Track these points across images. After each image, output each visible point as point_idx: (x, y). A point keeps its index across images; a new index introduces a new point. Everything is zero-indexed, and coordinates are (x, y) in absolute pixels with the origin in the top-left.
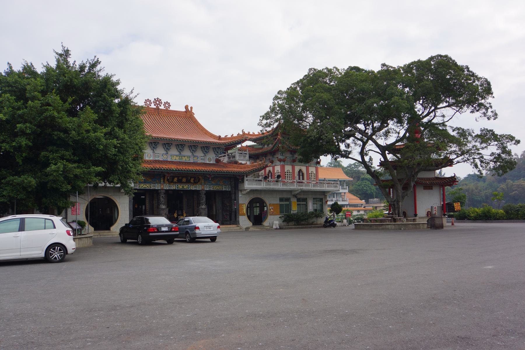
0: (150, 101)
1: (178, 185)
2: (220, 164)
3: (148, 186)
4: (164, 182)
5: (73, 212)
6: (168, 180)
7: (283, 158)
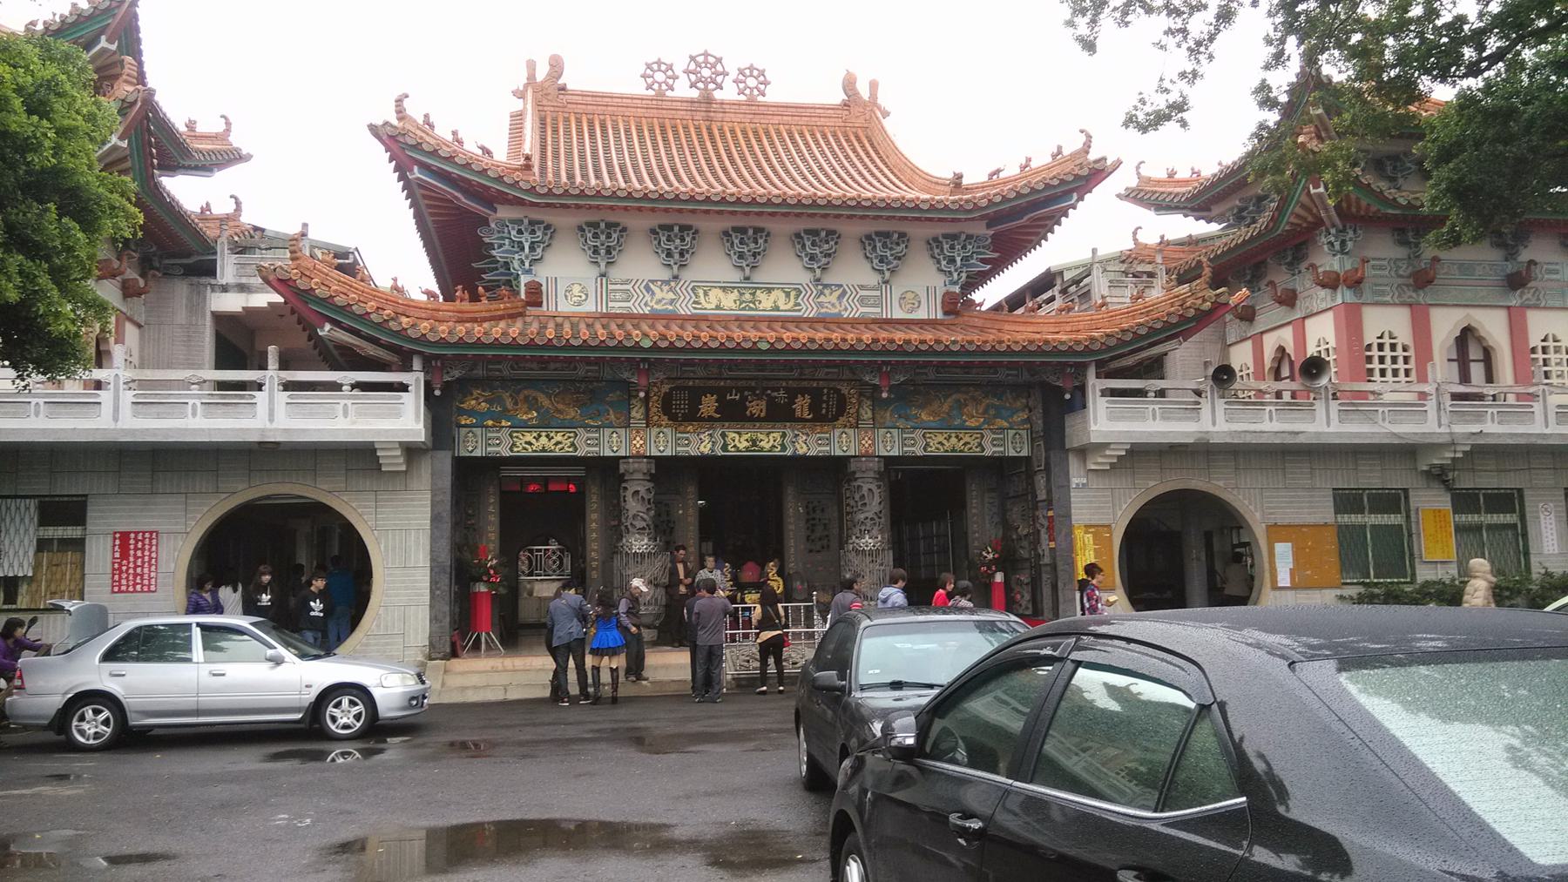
1: (724, 435)
2: (966, 319)
3: (557, 443)
4: (647, 418)
5: (120, 578)
6: (667, 409)
7: (1348, 267)
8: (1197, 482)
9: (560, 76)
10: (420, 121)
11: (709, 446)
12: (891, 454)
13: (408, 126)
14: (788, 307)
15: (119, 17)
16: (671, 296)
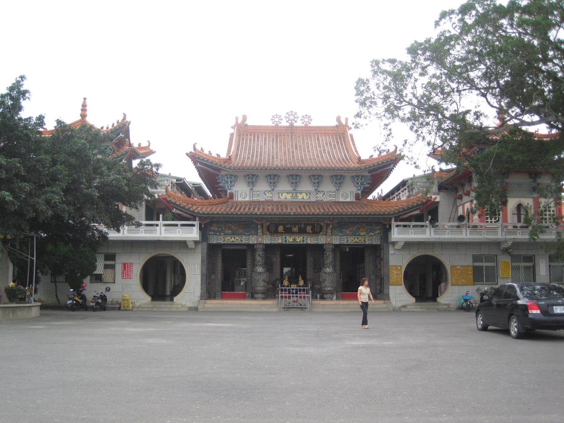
0: (309, 118)
1: (285, 238)
6: (268, 230)
8: (430, 253)
9: (245, 122)
10: (200, 150)
11: (281, 241)
12: (337, 243)
13: (196, 152)
14: (307, 198)
15: (125, 129)
16: (271, 195)
